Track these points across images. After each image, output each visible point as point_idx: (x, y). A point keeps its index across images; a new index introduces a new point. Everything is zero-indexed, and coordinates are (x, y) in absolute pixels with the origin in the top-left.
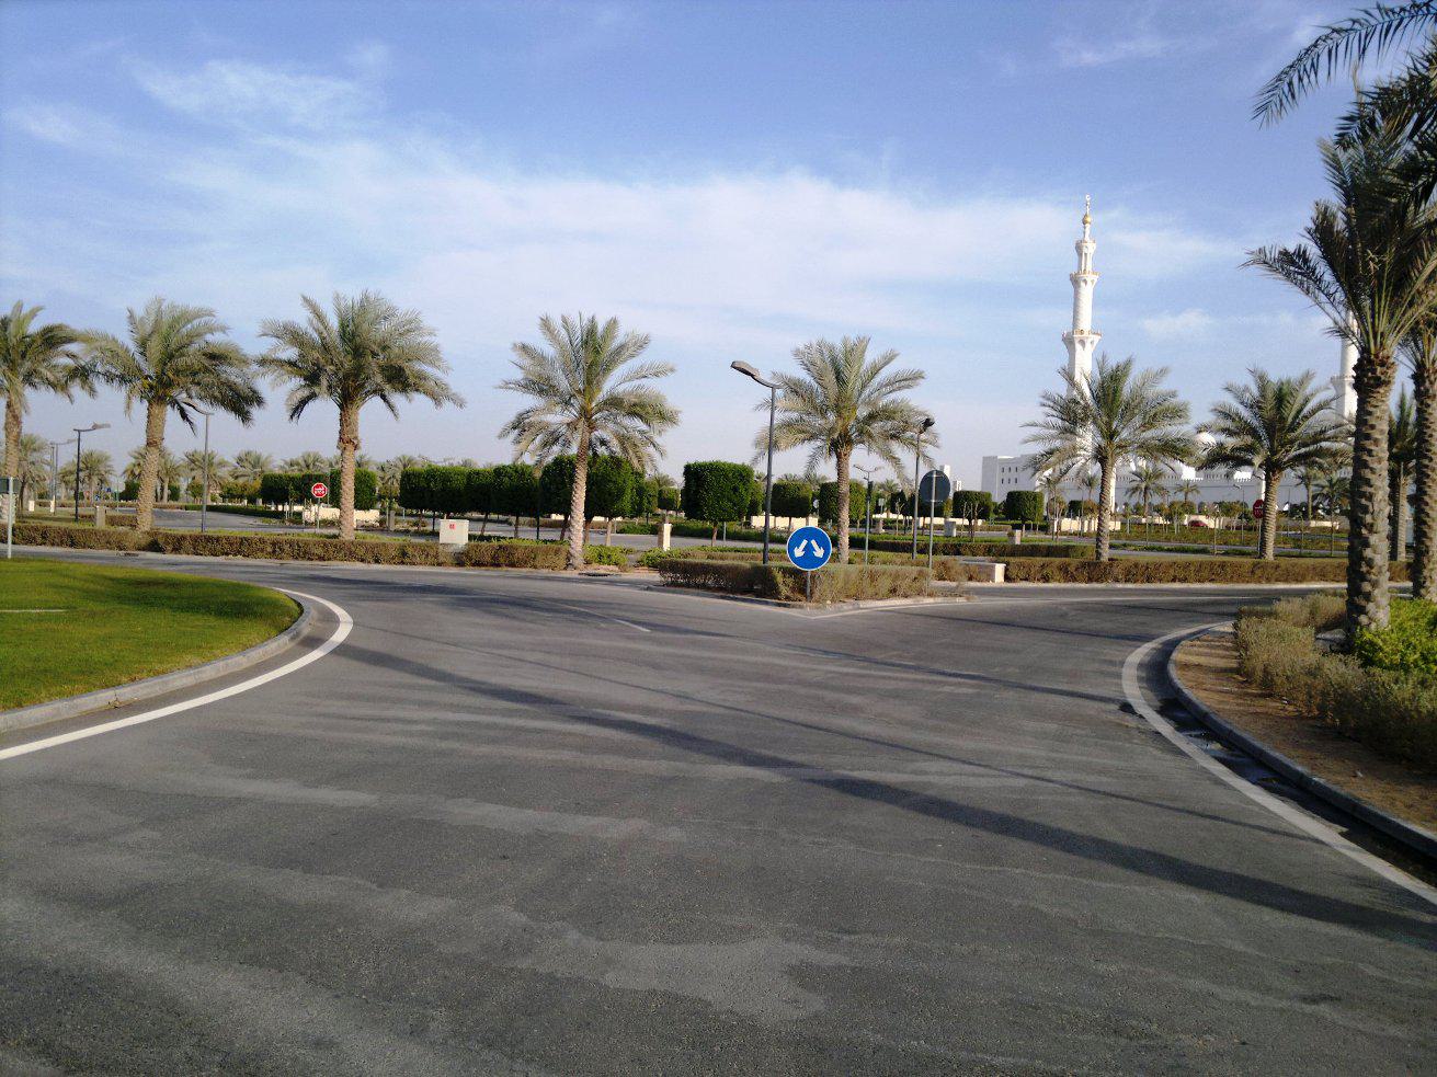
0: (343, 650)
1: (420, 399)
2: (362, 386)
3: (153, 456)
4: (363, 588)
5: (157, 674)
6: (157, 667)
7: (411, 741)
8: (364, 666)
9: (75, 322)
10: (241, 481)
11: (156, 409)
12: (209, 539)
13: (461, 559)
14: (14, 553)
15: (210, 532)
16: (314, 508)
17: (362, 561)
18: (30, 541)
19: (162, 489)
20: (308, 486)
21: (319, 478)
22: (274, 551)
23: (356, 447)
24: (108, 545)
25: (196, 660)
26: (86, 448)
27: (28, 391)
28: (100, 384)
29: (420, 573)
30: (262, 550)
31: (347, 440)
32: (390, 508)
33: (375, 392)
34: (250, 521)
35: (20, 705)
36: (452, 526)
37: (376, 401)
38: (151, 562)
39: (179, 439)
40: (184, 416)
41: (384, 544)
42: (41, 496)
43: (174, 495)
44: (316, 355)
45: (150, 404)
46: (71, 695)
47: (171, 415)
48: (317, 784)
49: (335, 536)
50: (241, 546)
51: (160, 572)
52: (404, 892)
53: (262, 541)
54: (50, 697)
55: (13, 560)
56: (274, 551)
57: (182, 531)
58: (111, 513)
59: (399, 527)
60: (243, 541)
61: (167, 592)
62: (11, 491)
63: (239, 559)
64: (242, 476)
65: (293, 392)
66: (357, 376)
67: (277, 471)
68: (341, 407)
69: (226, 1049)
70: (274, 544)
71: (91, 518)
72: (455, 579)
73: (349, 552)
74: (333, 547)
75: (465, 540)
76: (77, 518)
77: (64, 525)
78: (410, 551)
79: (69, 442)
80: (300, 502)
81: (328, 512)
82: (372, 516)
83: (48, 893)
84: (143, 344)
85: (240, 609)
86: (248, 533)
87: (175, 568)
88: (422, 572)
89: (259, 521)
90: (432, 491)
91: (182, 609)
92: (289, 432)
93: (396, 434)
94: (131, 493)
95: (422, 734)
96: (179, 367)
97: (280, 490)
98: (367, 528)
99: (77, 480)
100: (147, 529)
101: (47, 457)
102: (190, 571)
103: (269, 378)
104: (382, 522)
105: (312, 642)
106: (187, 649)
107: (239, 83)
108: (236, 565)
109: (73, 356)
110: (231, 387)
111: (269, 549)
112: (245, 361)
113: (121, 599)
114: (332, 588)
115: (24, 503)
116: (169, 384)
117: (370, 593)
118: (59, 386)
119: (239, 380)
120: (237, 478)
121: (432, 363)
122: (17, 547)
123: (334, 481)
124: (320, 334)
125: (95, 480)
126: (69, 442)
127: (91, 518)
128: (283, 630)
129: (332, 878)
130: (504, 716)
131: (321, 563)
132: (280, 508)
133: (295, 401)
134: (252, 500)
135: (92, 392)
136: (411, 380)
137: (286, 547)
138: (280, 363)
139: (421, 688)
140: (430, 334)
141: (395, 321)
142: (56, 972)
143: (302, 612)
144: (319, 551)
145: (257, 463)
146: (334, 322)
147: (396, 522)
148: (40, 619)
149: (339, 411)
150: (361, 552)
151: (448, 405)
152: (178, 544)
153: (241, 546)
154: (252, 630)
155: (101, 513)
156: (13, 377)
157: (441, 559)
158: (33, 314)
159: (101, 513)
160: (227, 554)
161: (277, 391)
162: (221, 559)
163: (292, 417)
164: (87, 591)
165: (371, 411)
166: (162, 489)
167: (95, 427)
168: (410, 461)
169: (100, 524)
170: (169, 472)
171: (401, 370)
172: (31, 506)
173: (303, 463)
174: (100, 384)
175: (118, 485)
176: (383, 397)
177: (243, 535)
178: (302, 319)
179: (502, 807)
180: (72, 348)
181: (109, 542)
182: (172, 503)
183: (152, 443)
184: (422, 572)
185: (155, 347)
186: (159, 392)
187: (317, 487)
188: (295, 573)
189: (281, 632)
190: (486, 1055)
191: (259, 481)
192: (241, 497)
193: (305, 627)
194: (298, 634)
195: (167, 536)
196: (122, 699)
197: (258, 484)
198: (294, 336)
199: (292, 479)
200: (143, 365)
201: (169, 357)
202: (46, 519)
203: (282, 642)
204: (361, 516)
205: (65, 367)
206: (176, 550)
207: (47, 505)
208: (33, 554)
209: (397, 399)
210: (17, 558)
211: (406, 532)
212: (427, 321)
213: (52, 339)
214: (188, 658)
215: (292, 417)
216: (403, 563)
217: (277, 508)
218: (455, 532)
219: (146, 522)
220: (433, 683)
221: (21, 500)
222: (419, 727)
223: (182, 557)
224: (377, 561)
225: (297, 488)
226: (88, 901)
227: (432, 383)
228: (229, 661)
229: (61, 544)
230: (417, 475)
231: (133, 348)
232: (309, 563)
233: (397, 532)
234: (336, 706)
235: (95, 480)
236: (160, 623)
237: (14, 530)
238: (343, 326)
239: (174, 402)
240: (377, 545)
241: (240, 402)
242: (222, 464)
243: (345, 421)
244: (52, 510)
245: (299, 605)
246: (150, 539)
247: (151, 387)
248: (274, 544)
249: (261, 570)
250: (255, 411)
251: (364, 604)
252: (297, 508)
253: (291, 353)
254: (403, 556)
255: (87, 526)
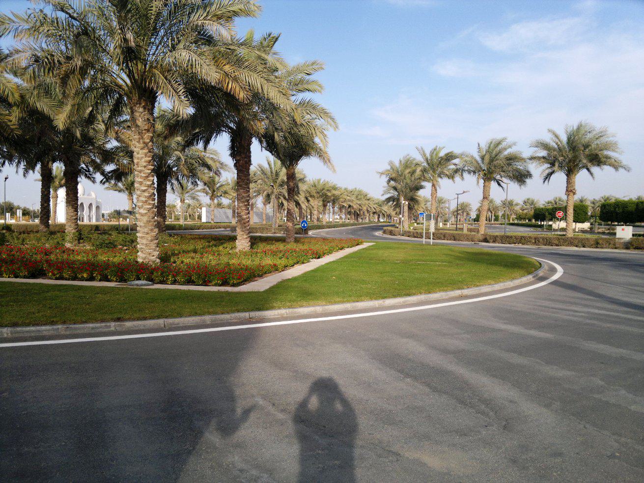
0: (555, 283)
1: (607, 168)
2: (577, 165)
3: (486, 203)
4: (573, 258)
5: (477, 286)
6: (478, 284)
7: (575, 319)
8: (564, 289)
9: (457, 151)
10: (525, 211)
11: (487, 184)
12: (508, 237)
13: (628, 245)
14: (433, 243)
15: (508, 234)
16: (558, 223)
17: (577, 246)
18: (440, 239)
19: (492, 216)
20: (555, 212)
21: (560, 209)
22: (536, 242)
23: (574, 194)
24: (468, 240)
25: (493, 282)
26: (460, 201)
27: (439, 179)
28: (466, 175)
29: (604, 252)
30: (530, 242)
31: (570, 191)
32: (595, 222)
33: (583, 167)
34: (528, 229)
35: (430, 293)
36: (623, 230)
37: (585, 171)
38: (483, 247)
39: (497, 194)
40: (499, 184)
41: (587, 239)
42: (445, 221)
43: (496, 219)
44: (555, 153)
45: (485, 181)
46: (446, 291)
47: (493, 184)
48: (531, 329)
49: (564, 235)
50: (521, 240)
51: (486, 250)
52: (555, 367)
53: (530, 237)
54: (440, 291)
55: (432, 245)
56: (536, 242)
57: (497, 234)
58: (470, 227)
59: (600, 230)
60: (522, 237)
61: (486, 257)
62: (432, 219)
63: (520, 245)
64: (526, 209)
65: (544, 171)
66: (574, 161)
67: (542, 206)
68: (567, 175)
69: (481, 396)
70: (535, 239)
71: (462, 229)
72: (618, 255)
73: (571, 242)
74: (563, 239)
75: (631, 236)
76: (456, 229)
77: (451, 232)
78: (600, 242)
79: (455, 199)
80: (551, 220)
81: (563, 224)
82: (586, 225)
83: (433, 347)
84: (483, 158)
85: (516, 265)
86: (525, 234)
87: (492, 249)
88: (607, 251)
89: (532, 229)
90: (617, 213)
91: (491, 264)
92: (544, 189)
93: (595, 186)
94: (477, 219)
95: (582, 316)
96: (497, 165)
97: (542, 215)
98: (583, 231)
99: (458, 214)
100: (483, 233)
101: (447, 205)
102: (499, 250)
103: (534, 164)
104: (591, 229)
105: (542, 279)
106: (489, 278)
107: (525, 32)
108: (519, 248)
109: (455, 165)
110: (517, 170)
111: (533, 241)
112: (523, 159)
113: (469, 260)
114: (560, 258)
115: (438, 224)
116: (491, 173)
117: (574, 260)
118: (451, 177)
119: (521, 168)
120: (523, 210)
121: (613, 151)
122: (435, 241)
123: (565, 209)
124: (557, 144)
125: (465, 214)
126: (455, 199)
127: (462, 229)
128: (529, 273)
129: (528, 358)
130: (623, 313)
131: (556, 247)
132: (542, 223)
133: (545, 174)
134: (530, 220)
135: (463, 179)
136: (603, 160)
137: (541, 240)
138: (539, 158)
139: (587, 299)
140: (612, 137)
141: (595, 132)
142: (433, 367)
143: (541, 266)
144: (557, 242)
145: (532, 203)
146: (564, 139)
147: (599, 228)
148: (439, 266)
149: (566, 177)
150: (576, 242)
151: (621, 170)
152: (495, 239)
153: (521, 240)
154: (517, 273)
155: (466, 227)
156: (434, 175)
157: (617, 246)
158: (441, 149)
159: (466, 227)
160: (515, 243)
161: (537, 170)
162: (513, 245)
163: (544, 182)
164: (457, 256)
165: (581, 176)
166: (492, 216)
167: (464, 192)
168: (608, 198)
169: (465, 231)
170: (493, 209)
171: (597, 155)
172: (441, 225)
173: (554, 202)
174: (466, 175)
175: (473, 215)
176: (588, 170)
177: (523, 235)
178: (548, 139)
179: (608, 346)
180: (456, 161)
181: (468, 238)
182: (496, 222)
183: (485, 198)
184: (607, 251)
185: (487, 158)
186: (488, 176)
187: (559, 213)
188: (544, 251)
189: (529, 274)
190: (571, 417)
191: (533, 211)
192: (525, 219)
193: (541, 273)
194: (537, 275)
195: (490, 235)
196: (464, 294)
197: (532, 212)
198: (545, 146)
199: (548, 210)
200: (482, 165)
201: (492, 160)
202: (446, 230)
203: (530, 278)
204: (580, 226)
205: (453, 169)
206: (494, 242)
207: (446, 224)
208: (440, 243)
209: (595, 170)
210: (434, 244)
211: (603, 233)
212: (611, 131)
213: (449, 157)
214: (489, 281)
215: (544, 182)
216: (597, 247)
217: (541, 223)
218: (625, 232)
219: (482, 231)
220: (592, 298)
221: (436, 223)
222: (581, 314)
223: (497, 245)
224: (584, 247)
225: (550, 214)
226: (445, 351)
227: (613, 160)
228: (505, 283)
229: (450, 239)
230: (609, 205)
231: (479, 159)
232: (552, 247)
233: (599, 233)
234: (547, 303)
235: (465, 214)
236: (481, 269)
237: (433, 234)
238: (569, 139)
239: (495, 179)
240: (584, 239)
241: (521, 177)
242: (517, 205)
243: (569, 182)
244: (448, 226)
245: (540, 264)
246: (484, 237)
247: (485, 174)
248: (535, 239)
249: (522, 250)
250: (528, 181)
251: (571, 265)
252: (550, 223)
253: (543, 153)
254: (597, 244)
255: (460, 232)
